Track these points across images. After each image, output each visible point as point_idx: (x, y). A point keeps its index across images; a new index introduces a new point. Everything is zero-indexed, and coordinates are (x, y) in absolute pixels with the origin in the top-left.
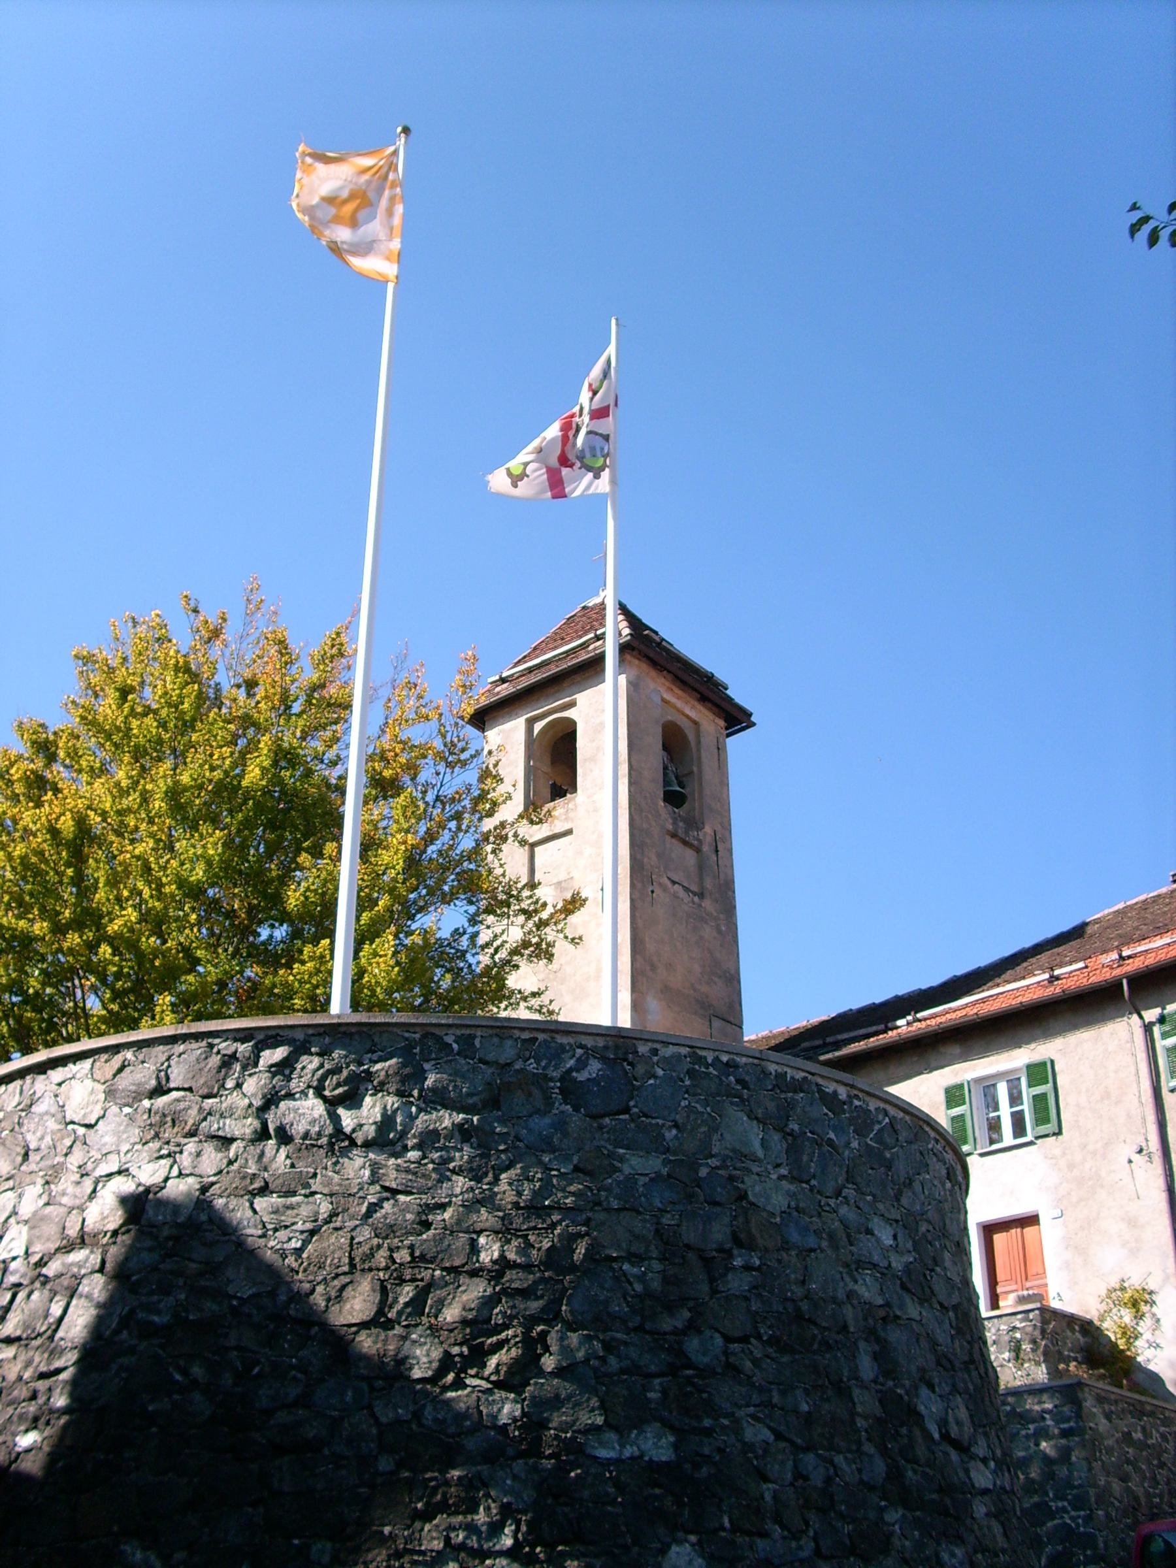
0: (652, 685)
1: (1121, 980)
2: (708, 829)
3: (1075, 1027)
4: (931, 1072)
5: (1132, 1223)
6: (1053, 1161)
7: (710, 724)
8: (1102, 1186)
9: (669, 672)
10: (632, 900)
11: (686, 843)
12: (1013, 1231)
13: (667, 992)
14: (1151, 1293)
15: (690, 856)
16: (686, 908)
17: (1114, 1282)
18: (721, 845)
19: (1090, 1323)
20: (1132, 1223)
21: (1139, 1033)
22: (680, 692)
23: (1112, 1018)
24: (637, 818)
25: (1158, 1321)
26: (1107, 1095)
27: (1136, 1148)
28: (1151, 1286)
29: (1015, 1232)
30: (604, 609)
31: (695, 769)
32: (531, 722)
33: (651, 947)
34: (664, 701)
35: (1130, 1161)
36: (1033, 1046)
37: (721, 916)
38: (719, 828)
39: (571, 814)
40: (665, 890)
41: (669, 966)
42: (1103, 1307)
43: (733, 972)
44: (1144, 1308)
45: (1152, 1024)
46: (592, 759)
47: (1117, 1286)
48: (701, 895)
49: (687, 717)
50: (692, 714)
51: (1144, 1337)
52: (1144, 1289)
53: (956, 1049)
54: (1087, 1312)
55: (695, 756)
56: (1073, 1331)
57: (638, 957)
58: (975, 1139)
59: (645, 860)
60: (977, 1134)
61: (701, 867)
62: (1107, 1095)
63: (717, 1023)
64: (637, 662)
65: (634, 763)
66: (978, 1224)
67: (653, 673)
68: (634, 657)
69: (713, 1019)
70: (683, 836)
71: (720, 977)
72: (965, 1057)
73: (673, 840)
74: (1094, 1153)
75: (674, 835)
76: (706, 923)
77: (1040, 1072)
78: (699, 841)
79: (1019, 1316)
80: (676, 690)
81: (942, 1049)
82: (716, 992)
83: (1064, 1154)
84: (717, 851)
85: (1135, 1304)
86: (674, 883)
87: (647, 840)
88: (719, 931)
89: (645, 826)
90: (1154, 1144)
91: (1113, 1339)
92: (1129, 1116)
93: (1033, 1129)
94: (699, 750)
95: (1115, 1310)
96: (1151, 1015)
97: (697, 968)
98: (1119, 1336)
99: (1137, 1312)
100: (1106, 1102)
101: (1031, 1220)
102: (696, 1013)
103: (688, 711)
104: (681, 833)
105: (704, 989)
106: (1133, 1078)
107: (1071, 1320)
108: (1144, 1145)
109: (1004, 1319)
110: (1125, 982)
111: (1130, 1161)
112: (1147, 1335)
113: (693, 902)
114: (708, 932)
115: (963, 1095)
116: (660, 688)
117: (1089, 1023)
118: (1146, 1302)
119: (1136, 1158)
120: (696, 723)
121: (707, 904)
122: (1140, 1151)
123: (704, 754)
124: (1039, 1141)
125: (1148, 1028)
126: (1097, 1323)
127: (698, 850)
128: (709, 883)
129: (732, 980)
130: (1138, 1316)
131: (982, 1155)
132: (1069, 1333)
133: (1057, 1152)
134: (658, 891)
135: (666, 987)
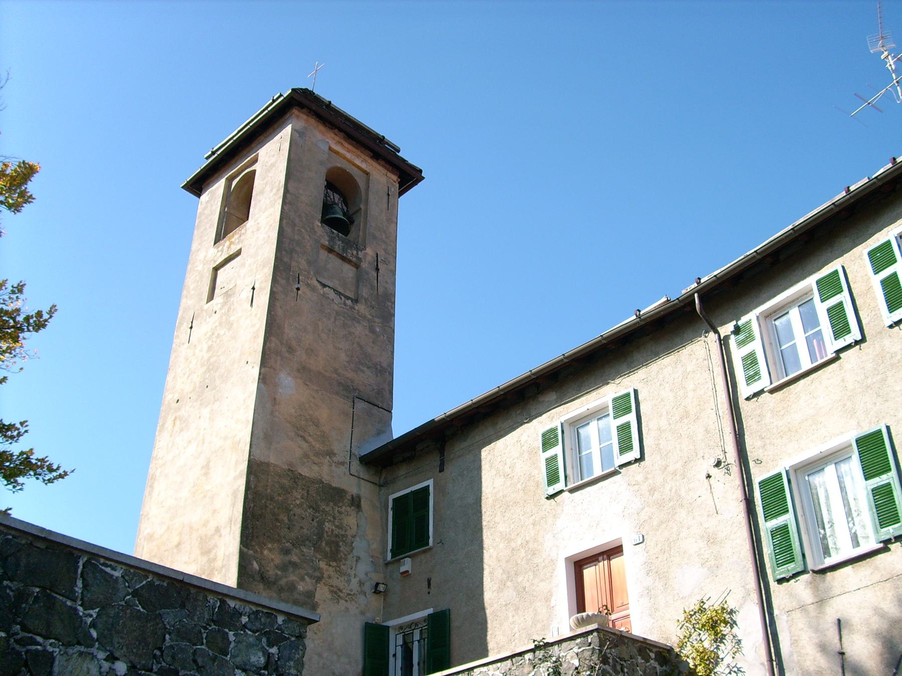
0: (319, 136)
1: (693, 294)
2: (369, 251)
3: (656, 355)
4: (531, 420)
5: (711, 540)
6: (636, 487)
7: (381, 178)
8: (682, 506)
9: (340, 130)
10: (272, 293)
11: (344, 259)
12: (601, 564)
13: (304, 372)
14: (731, 612)
15: (348, 271)
16: (336, 307)
17: (693, 605)
18: (385, 264)
19: (670, 650)
20: (711, 540)
21: (715, 347)
22: (350, 147)
23: (691, 340)
24: (288, 230)
25: (739, 642)
26: (686, 414)
27: (713, 461)
28: (731, 605)
29: (602, 565)
30: (788, 532)
31: (362, 206)
32: (230, 180)
33: (289, 332)
34: (330, 149)
35: (709, 476)
36: (617, 381)
37: (377, 320)
38: (382, 254)
39: (243, 237)
40: (313, 289)
41: (310, 352)
42: (681, 633)
43: (385, 365)
44: (724, 629)
45: (727, 338)
46: (262, 192)
47: (697, 608)
48: (356, 301)
49: (358, 167)
50: (364, 166)
51: (726, 662)
52: (723, 609)
53: (552, 396)
54: (667, 639)
55: (363, 198)
56: (647, 659)
57: (273, 339)
58: (566, 477)
59: (293, 264)
60: (569, 472)
61: (359, 279)
62: (686, 414)
63: (360, 405)
64: (305, 117)
65: (291, 189)
66: (567, 559)
67: (322, 128)
68: (304, 113)
69: (356, 400)
70: (340, 252)
71: (368, 368)
72: (560, 402)
73: (330, 255)
74: (674, 473)
75: (330, 250)
76: (358, 322)
77: (622, 405)
78: (359, 259)
79: (578, 640)
80: (346, 145)
81: (541, 399)
82: (366, 379)
83: (646, 478)
84: (377, 269)
85: (713, 626)
86: (324, 286)
87: (298, 249)
88: (373, 331)
89: (296, 237)
90: (732, 456)
91: (691, 665)
92: (707, 431)
93: (774, 572)
94: (367, 195)
95: (695, 636)
96: (726, 329)
97: (343, 357)
98: (698, 662)
99: (716, 634)
100: (685, 421)
101: (615, 551)
102: (337, 393)
103: (358, 162)
104: (336, 248)
105: (350, 375)
106: (710, 393)
107: (644, 646)
108: (721, 457)
109: (564, 645)
110: (696, 295)
111: (709, 476)
112: (728, 660)
113: (345, 304)
114: (359, 330)
115: (556, 436)
116: (326, 141)
117: (669, 348)
118: (726, 623)
119: (714, 472)
120: (367, 174)
121: (361, 308)
122: (718, 464)
123: (371, 197)
124: (623, 470)
125: (724, 343)
126: (677, 650)
127: (357, 266)
128: (365, 292)
129: (385, 372)
130: (719, 639)
131: (572, 491)
132: (640, 660)
133: (640, 478)
134: (303, 288)
135: (304, 368)
